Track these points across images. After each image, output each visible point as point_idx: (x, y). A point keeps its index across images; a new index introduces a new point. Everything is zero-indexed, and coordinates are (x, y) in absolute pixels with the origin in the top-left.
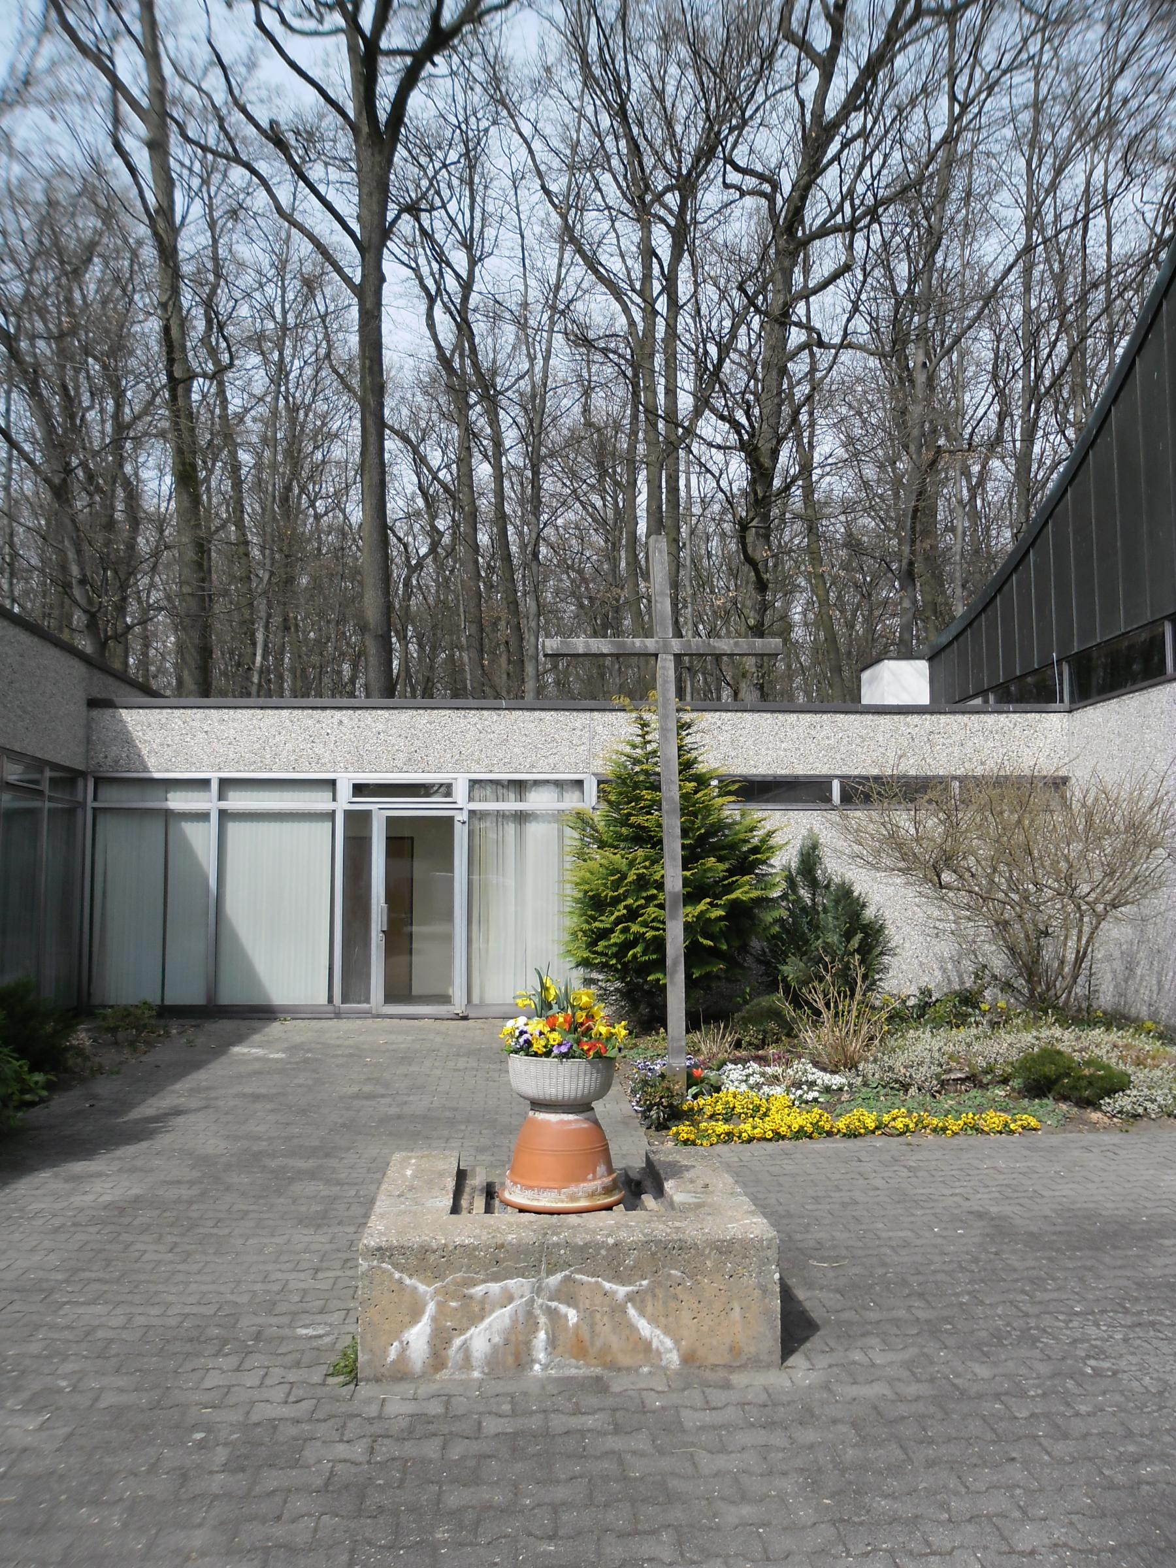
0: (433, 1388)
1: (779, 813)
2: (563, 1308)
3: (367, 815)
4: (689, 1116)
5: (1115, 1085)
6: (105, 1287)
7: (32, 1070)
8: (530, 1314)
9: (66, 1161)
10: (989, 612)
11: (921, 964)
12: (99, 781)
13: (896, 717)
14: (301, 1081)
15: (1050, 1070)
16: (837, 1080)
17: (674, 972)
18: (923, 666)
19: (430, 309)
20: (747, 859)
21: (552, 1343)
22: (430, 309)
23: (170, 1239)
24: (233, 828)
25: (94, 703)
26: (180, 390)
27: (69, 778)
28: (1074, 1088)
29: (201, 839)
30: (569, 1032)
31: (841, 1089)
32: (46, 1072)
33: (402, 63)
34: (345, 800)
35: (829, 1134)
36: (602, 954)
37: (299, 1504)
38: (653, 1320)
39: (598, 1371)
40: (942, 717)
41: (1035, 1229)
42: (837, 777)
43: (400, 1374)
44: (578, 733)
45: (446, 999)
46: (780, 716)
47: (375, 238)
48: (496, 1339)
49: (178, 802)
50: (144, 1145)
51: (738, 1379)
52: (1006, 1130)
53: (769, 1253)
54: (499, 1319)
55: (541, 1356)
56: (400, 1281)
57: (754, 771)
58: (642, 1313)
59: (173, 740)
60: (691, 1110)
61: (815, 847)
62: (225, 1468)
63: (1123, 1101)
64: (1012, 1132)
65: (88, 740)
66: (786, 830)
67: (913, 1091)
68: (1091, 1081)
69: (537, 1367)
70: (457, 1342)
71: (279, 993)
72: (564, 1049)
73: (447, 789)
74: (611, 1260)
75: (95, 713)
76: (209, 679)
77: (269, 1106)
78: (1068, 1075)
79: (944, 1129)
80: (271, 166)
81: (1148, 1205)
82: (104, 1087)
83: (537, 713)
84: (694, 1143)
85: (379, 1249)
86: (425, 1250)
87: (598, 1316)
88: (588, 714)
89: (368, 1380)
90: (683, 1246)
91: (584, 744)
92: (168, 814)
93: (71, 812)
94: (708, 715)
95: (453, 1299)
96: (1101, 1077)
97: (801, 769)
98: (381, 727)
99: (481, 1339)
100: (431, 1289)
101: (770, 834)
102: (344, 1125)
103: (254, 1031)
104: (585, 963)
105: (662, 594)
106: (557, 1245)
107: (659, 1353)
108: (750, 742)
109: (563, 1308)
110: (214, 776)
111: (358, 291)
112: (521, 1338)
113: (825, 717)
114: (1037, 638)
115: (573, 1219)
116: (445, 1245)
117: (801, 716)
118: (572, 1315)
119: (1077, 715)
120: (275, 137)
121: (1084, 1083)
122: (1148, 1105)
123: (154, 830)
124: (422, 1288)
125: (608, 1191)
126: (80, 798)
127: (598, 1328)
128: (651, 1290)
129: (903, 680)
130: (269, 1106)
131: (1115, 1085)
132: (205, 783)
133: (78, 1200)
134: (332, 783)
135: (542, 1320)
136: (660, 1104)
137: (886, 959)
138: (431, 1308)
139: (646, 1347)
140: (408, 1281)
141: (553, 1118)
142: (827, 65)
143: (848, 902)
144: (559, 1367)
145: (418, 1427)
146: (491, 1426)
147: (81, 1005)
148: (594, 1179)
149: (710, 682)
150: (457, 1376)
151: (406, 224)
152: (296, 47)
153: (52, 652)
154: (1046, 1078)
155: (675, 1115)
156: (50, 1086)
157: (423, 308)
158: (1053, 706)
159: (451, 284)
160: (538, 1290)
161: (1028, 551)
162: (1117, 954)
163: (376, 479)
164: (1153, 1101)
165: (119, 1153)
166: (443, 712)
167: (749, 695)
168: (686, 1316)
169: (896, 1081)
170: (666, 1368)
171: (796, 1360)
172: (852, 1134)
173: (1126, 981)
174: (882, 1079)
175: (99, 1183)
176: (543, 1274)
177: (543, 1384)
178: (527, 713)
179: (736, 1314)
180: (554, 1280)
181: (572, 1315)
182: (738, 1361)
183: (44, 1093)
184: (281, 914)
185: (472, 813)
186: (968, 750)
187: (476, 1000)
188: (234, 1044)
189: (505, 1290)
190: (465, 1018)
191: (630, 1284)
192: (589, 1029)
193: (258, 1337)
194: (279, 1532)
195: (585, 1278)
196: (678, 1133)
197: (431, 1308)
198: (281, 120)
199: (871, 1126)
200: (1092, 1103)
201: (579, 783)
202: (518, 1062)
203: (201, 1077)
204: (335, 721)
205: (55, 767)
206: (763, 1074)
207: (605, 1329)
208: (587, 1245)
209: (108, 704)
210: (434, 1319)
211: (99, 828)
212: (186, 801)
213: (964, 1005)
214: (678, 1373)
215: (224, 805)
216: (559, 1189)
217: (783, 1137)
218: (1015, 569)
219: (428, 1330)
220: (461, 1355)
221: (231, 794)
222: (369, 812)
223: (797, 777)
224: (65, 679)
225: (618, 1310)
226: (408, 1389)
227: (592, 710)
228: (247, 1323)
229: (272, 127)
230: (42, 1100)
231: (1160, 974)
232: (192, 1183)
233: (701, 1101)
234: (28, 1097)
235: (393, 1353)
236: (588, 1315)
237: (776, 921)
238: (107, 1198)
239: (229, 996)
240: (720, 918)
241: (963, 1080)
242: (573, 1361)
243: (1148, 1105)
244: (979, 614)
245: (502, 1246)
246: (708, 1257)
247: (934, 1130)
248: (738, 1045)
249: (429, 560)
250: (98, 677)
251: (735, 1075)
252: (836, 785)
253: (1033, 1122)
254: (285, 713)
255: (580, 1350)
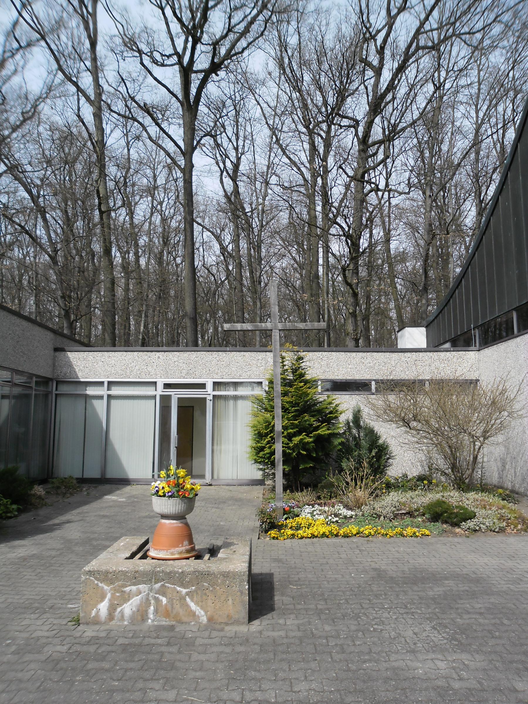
0: (107, 627)
1: (348, 396)
2: (161, 597)
3: (169, 397)
4: (280, 527)
5: (469, 516)
6: (3, 588)
7: (12, 504)
8: (147, 599)
9: (14, 540)
10: (448, 306)
11: (412, 463)
12: (58, 383)
13: (400, 354)
14: (126, 510)
15: (439, 510)
16: (349, 513)
17: (278, 465)
18: (423, 330)
19: (222, 175)
20: (328, 417)
21: (156, 611)
22: (222, 175)
23: (39, 571)
24: (113, 402)
25: (56, 350)
26: (104, 216)
27: (45, 381)
28: (449, 518)
29: (100, 407)
30: (175, 487)
31: (351, 517)
32: (18, 504)
33: (201, 76)
34: (160, 391)
35: (337, 535)
36: (261, 457)
37: (33, 666)
38: (197, 604)
39: (174, 623)
40: (421, 353)
41: (394, 576)
42: (374, 380)
43: (96, 622)
44: (260, 361)
45: (203, 477)
46: (348, 354)
47: (190, 149)
48: (134, 609)
49: (91, 391)
50: (48, 534)
51: (227, 628)
52: (414, 535)
53: (244, 577)
54: (135, 601)
55: (151, 616)
56: (97, 585)
57: (337, 378)
58: (192, 600)
59: (89, 365)
60: (282, 525)
61: (359, 411)
62: (13, 653)
63: (470, 524)
64: (417, 536)
65: (54, 365)
66: (346, 404)
67: (382, 518)
68: (457, 515)
69: (150, 621)
70: (119, 610)
71: (132, 474)
72: (170, 494)
73: (203, 386)
74: (180, 579)
75: (57, 354)
76: (117, 339)
77: (107, 520)
78: (446, 512)
79: (387, 534)
80: (147, 121)
81: (452, 567)
82: (43, 512)
83: (242, 353)
84: (277, 538)
85: (90, 571)
86: (107, 572)
87: (175, 601)
88: (264, 353)
89: (83, 624)
90: (209, 574)
91: (255, 368)
92: (86, 396)
93: (46, 395)
94: (311, 354)
95: (118, 592)
96: (461, 513)
97: (358, 376)
98: (176, 359)
99: (128, 609)
100: (109, 588)
101: (337, 406)
102: (134, 529)
103: (118, 489)
104: (256, 462)
105: (274, 304)
106: (159, 572)
107: (198, 617)
108: (335, 365)
109: (161, 597)
110: (106, 380)
111: (183, 171)
112: (144, 609)
113: (368, 354)
114: (470, 318)
115: (171, 562)
116: (115, 571)
117: (358, 353)
118: (164, 600)
119: (482, 352)
120: (146, 109)
121: (453, 516)
122: (482, 526)
123: (81, 403)
124: (106, 587)
125: (188, 551)
126: (50, 390)
127: (175, 606)
128: (196, 591)
129: (415, 337)
130: (107, 520)
131: (469, 516)
132: (102, 383)
133: (10, 555)
134: (155, 383)
135: (152, 602)
136: (266, 522)
137: (390, 461)
138: (109, 596)
139: (193, 614)
140: (100, 585)
141: (167, 522)
142: (378, 72)
143: (372, 436)
144: (159, 621)
145: (94, 640)
146: (120, 641)
147: (47, 476)
148: (182, 546)
149: (329, 339)
150: (118, 623)
151: (208, 141)
152: (157, 71)
153: (37, 328)
154: (437, 513)
155: (273, 526)
156: (19, 510)
157: (219, 174)
158: (471, 348)
159: (229, 164)
160: (151, 590)
161: (461, 280)
162: (499, 459)
163: (190, 251)
164: (484, 524)
165: (35, 537)
166: (202, 353)
167: (351, 343)
168: (210, 602)
169: (376, 514)
170: (201, 623)
171: (256, 622)
172: (346, 536)
173: (502, 471)
174: (370, 513)
175: (24, 548)
176: (153, 583)
177: (150, 627)
178: (238, 353)
179: (230, 602)
180: (158, 586)
181: (164, 600)
182: (231, 621)
183: (16, 513)
184: (133, 439)
185: (214, 396)
186: (433, 368)
187: (215, 477)
188: (106, 495)
189: (138, 589)
190: (210, 485)
191: (188, 588)
192: (184, 486)
193: (51, 608)
194: (20, 675)
195: (170, 585)
196: (270, 534)
197: (109, 596)
198: (148, 103)
199: (355, 532)
200: (457, 525)
201: (260, 383)
202: (155, 499)
203: (86, 508)
204: (157, 357)
205: (38, 376)
206: (320, 510)
207: (177, 606)
208: (171, 572)
209: (63, 350)
210: (110, 600)
211: (58, 401)
212: (94, 391)
213: (424, 481)
214: (205, 625)
215: (110, 392)
216: (167, 550)
217: (316, 537)
218: (457, 287)
219: (108, 604)
220: (120, 615)
221: (113, 388)
222: (170, 396)
223: (356, 380)
224: (44, 340)
225: (182, 599)
226: (97, 627)
227: (266, 351)
228: (49, 603)
229: (144, 105)
230: (16, 516)
231: (515, 468)
232: (58, 550)
233: (288, 521)
234: (9, 515)
235: (93, 613)
236: (171, 601)
237: (340, 444)
238: (22, 555)
239: (111, 474)
240: (312, 442)
241: (405, 514)
242: (164, 619)
243: (482, 526)
244: (444, 308)
245: (137, 571)
246: (219, 578)
247: (383, 535)
248: (319, 498)
249: (226, 282)
250: (59, 338)
251: (307, 511)
252: (373, 383)
253: (427, 532)
254: (136, 353)
255: (167, 614)
